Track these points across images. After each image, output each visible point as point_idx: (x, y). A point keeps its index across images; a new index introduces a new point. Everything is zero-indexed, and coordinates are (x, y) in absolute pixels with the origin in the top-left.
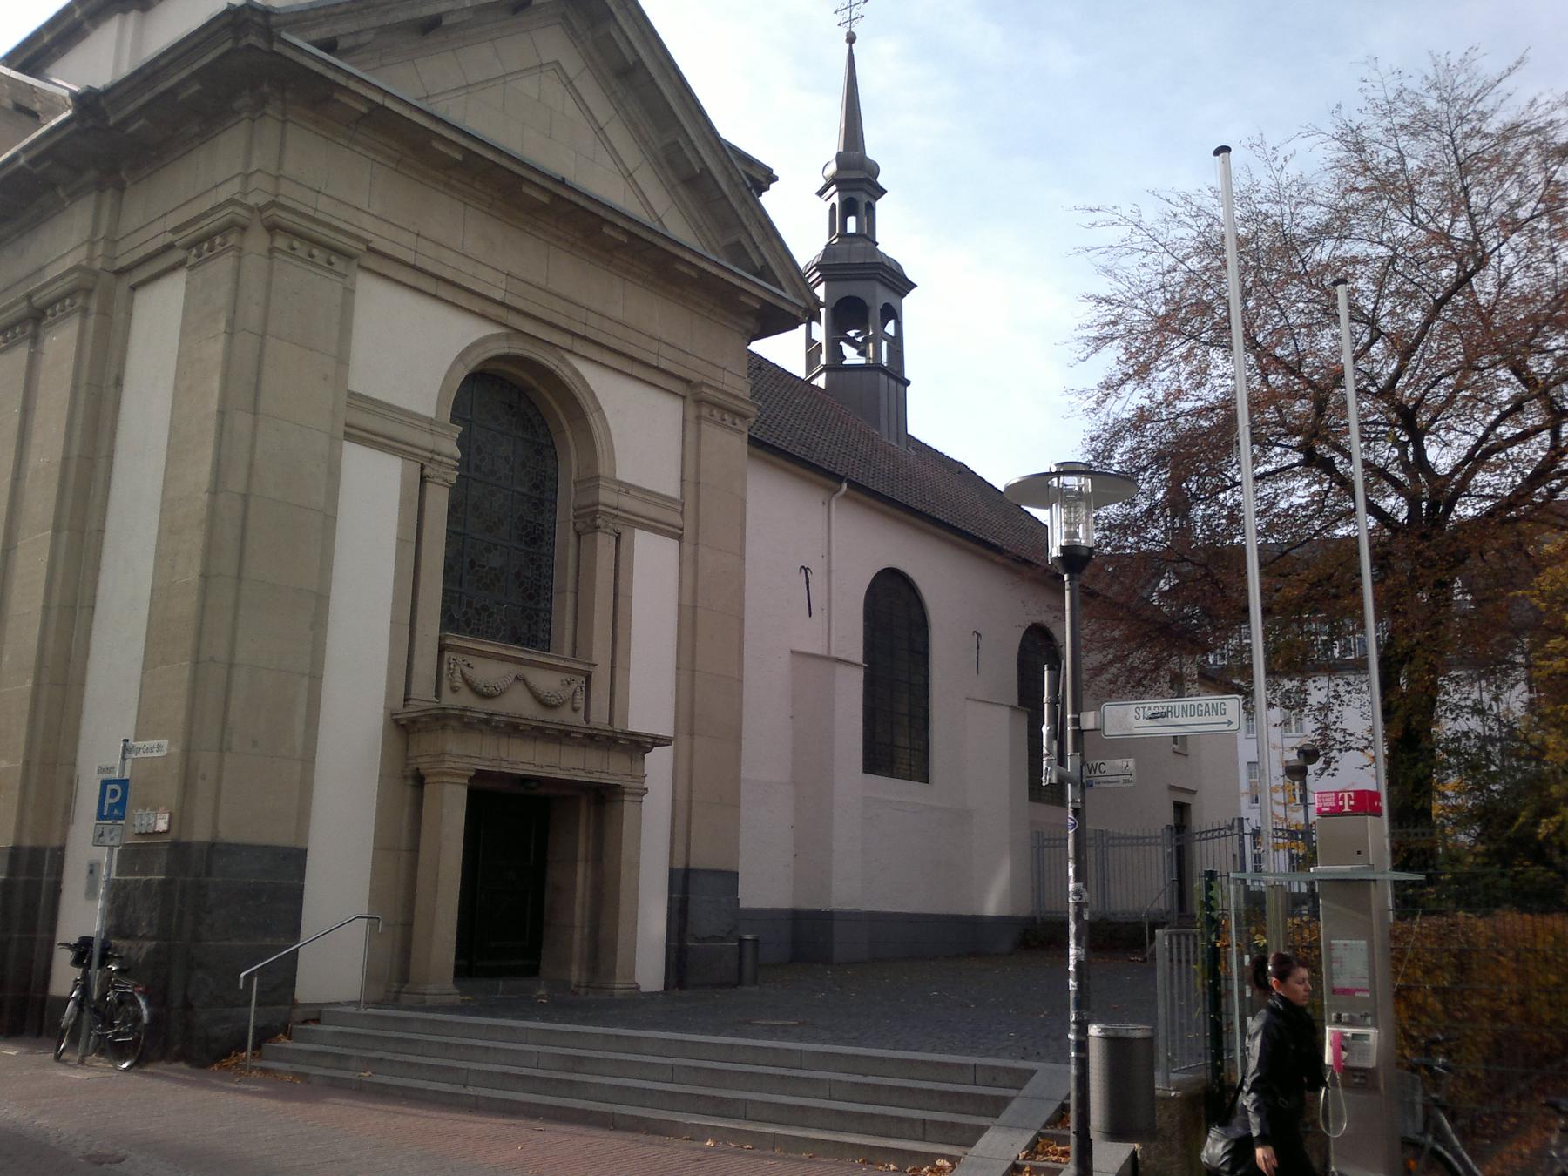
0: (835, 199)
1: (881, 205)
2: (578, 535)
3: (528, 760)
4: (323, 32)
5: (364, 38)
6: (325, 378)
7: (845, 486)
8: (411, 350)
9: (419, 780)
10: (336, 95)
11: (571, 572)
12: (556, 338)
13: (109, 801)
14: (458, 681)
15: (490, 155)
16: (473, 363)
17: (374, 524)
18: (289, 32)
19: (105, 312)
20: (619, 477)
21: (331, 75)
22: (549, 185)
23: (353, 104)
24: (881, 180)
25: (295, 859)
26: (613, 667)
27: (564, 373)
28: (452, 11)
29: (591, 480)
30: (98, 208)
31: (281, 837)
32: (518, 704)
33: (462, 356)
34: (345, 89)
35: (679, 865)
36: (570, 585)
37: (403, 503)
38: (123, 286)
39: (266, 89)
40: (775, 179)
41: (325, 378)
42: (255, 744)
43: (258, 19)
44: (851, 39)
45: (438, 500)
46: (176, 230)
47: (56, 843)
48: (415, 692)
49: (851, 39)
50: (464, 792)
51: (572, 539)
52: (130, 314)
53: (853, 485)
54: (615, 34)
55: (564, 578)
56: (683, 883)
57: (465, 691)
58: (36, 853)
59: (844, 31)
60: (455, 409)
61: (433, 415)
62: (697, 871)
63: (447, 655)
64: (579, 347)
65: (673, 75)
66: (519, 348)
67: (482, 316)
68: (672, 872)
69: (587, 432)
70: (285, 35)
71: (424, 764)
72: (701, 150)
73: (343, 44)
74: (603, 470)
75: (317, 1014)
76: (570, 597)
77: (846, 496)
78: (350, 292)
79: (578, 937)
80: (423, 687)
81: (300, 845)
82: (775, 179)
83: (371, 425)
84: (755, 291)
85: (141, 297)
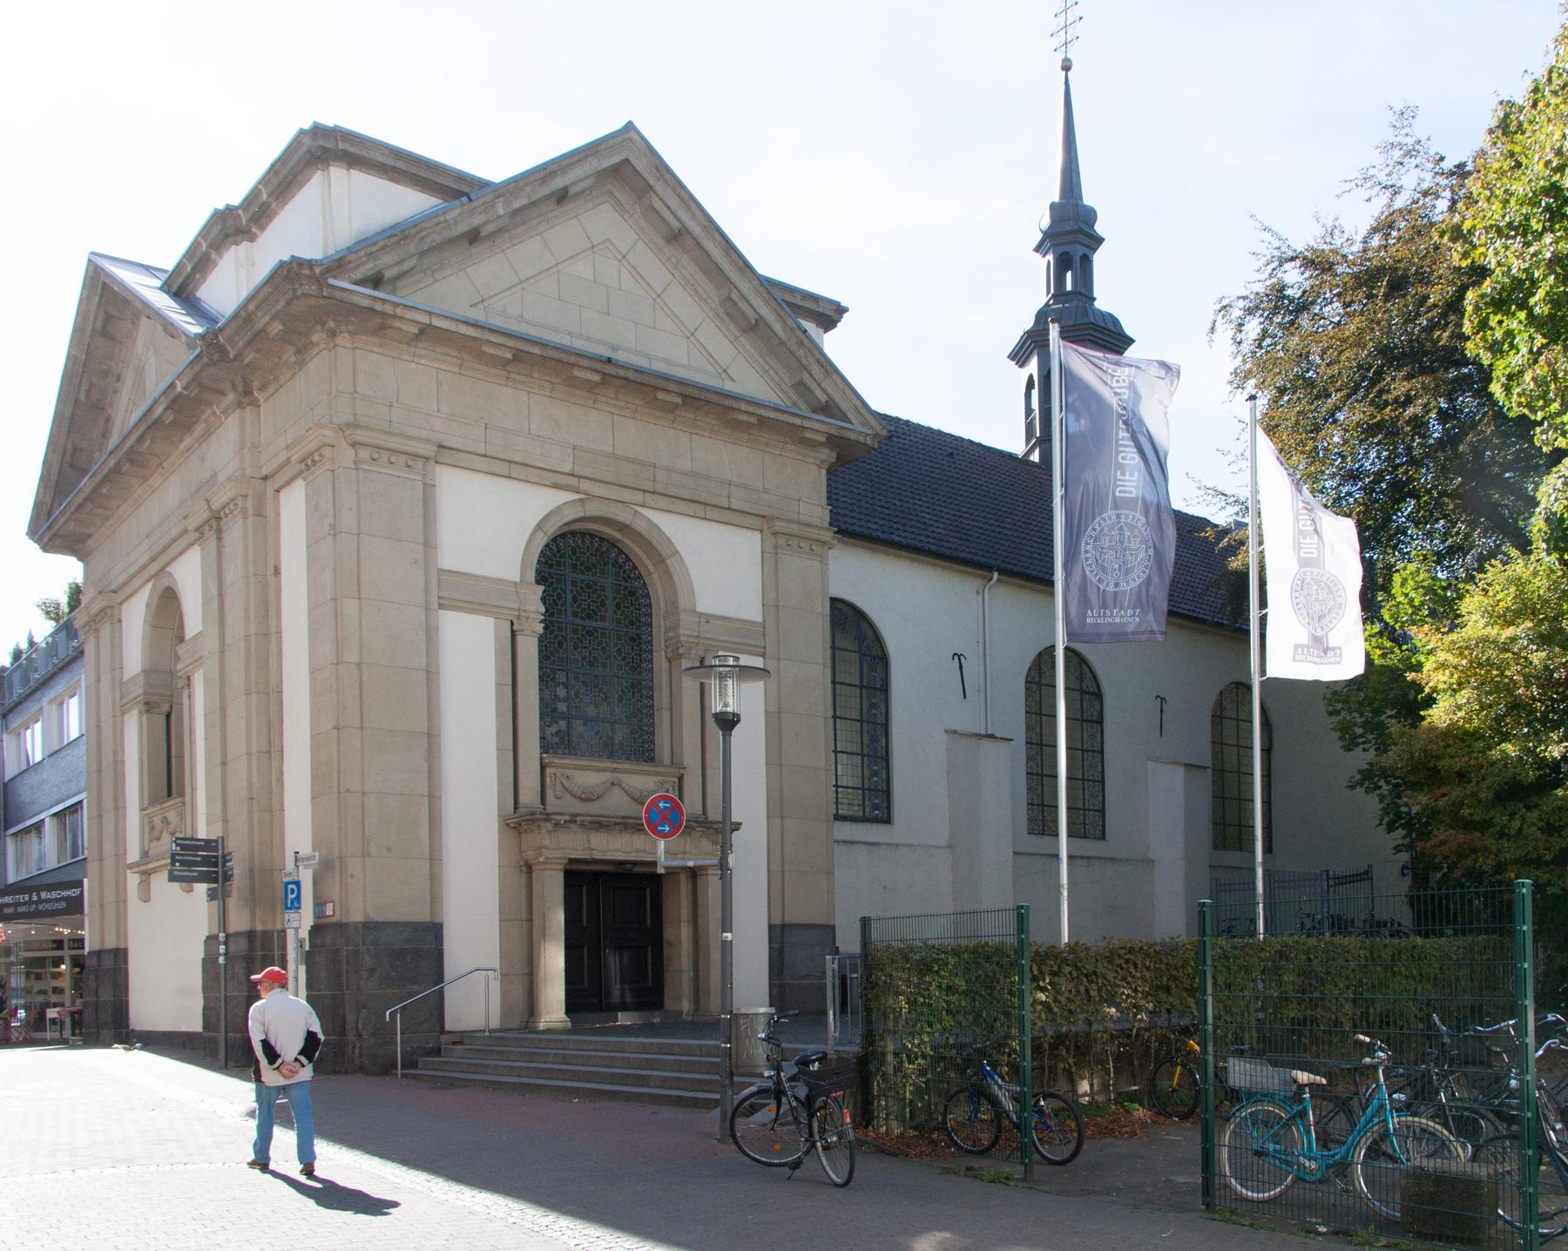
0: (1050, 257)
1: (1099, 259)
2: (670, 661)
3: (615, 848)
4: (367, 269)
5: (407, 265)
6: (416, 562)
7: (996, 575)
8: (493, 526)
9: (529, 868)
10: (389, 322)
11: (665, 692)
12: (627, 495)
13: (291, 896)
14: (559, 787)
15: (537, 350)
16: (552, 529)
17: (474, 674)
18: (335, 277)
19: (260, 514)
20: (701, 608)
21: (378, 307)
22: (598, 366)
23: (405, 327)
24: (1100, 228)
25: (435, 931)
26: (704, 769)
27: (640, 526)
28: (487, 222)
29: (674, 610)
30: (242, 422)
31: (422, 915)
32: (616, 804)
33: (539, 526)
34: (394, 316)
35: (777, 921)
36: (665, 702)
37: (499, 653)
38: (270, 487)
39: (331, 324)
40: (845, 310)
41: (416, 562)
42: (389, 849)
43: (306, 272)
44: (1067, 67)
45: (529, 650)
46: (289, 447)
47: (279, 927)
48: (522, 799)
49: (1067, 67)
50: (560, 877)
51: (665, 665)
52: (278, 514)
53: (1002, 571)
54: (658, 205)
55: (662, 698)
56: (779, 935)
57: (568, 797)
58: (267, 935)
59: (1060, 56)
60: (538, 572)
61: (518, 579)
62: (790, 925)
63: (548, 771)
64: (649, 499)
65: (717, 236)
66: (593, 509)
67: (556, 486)
68: (771, 927)
69: (667, 573)
70: (332, 281)
71: (530, 854)
72: (754, 302)
73: (388, 274)
74: (683, 603)
75: (461, 1038)
76: (666, 714)
77: (999, 580)
78: (429, 489)
79: (686, 977)
80: (529, 795)
81: (437, 920)
82: (845, 310)
83: (463, 593)
84: (818, 426)
85: (282, 494)
